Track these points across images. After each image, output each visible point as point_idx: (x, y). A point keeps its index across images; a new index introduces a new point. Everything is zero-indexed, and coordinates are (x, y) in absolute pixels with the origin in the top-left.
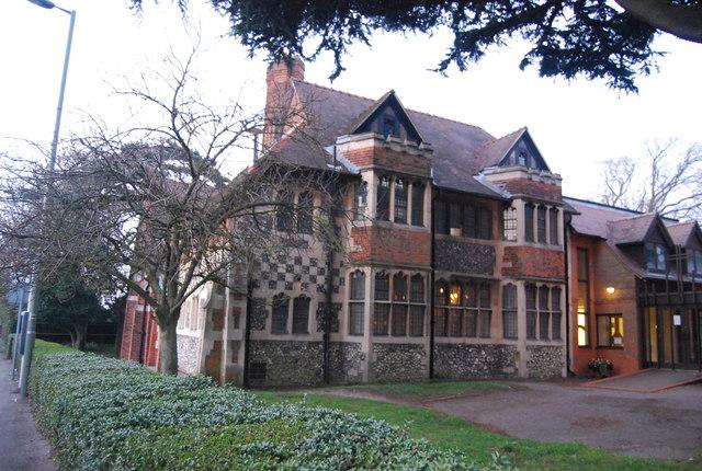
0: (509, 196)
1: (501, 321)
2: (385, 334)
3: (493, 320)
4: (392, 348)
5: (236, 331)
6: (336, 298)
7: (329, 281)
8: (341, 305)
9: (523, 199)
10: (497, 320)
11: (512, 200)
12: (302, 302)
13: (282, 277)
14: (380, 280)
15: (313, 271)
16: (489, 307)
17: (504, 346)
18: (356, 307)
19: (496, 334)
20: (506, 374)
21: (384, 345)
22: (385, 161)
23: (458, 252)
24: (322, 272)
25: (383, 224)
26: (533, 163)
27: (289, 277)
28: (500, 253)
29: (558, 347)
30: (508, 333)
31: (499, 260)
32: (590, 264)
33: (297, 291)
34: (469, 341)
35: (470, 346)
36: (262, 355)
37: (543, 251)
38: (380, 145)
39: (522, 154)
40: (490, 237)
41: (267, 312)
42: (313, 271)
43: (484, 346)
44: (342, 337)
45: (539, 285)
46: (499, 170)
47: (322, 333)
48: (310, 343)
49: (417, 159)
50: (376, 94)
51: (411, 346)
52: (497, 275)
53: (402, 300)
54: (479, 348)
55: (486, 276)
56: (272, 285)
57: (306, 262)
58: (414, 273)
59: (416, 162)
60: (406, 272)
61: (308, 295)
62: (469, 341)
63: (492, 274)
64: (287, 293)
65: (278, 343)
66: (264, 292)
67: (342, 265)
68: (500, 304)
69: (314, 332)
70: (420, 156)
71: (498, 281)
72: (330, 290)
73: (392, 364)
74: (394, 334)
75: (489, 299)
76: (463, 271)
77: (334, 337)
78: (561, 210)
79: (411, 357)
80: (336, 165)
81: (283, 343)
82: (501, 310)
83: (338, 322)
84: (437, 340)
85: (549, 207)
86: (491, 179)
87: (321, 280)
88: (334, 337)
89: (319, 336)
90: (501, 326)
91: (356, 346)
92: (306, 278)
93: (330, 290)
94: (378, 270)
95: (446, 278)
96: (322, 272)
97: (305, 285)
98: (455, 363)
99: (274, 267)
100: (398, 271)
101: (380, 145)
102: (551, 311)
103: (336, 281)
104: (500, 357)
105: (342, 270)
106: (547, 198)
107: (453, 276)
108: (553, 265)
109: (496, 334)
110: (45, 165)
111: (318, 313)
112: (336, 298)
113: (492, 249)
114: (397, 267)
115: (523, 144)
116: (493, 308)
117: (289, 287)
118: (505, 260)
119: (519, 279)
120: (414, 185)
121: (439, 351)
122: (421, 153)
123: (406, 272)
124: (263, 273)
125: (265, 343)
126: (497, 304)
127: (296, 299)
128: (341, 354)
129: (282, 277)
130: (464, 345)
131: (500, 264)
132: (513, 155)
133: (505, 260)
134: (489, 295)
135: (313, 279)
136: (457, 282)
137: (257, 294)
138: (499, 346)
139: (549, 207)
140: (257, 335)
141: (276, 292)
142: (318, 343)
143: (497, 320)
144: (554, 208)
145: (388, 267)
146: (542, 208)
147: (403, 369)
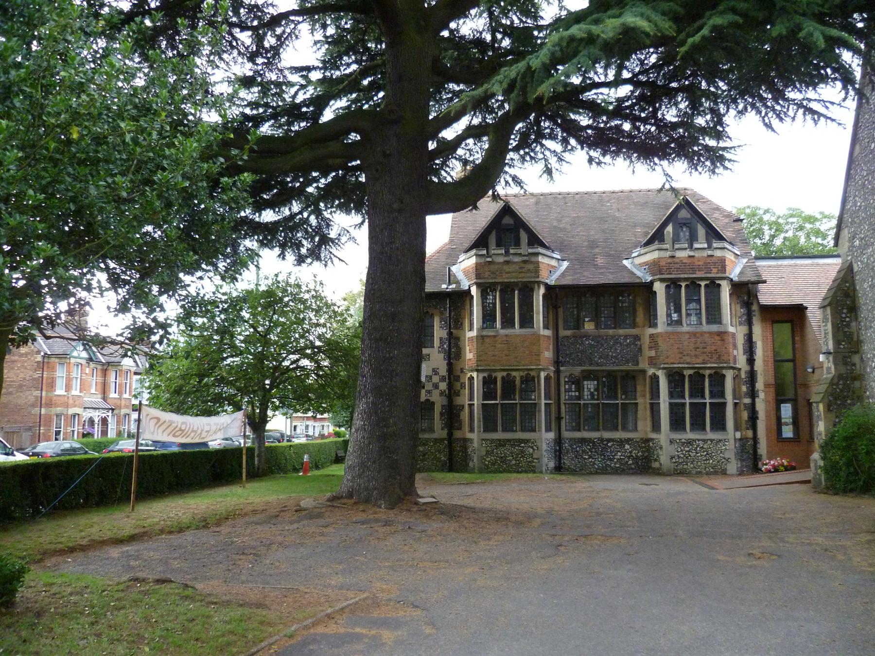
0: (649, 279)
1: (648, 412)
2: (495, 430)
4: (501, 443)
6: (458, 401)
7: (450, 386)
8: (463, 406)
9: (662, 280)
10: (644, 412)
11: (652, 283)
16: (636, 399)
17: (652, 440)
18: (654, 409)
21: (492, 441)
23: (591, 346)
24: (443, 379)
25: (489, 332)
26: (701, 231)
29: (720, 441)
32: (797, 338)
34: (607, 435)
35: (609, 440)
37: (694, 334)
38: (482, 260)
39: (681, 225)
40: (634, 325)
42: (436, 379)
46: (643, 251)
47: (446, 431)
48: (436, 439)
49: (523, 265)
52: (643, 364)
53: (531, 400)
54: (621, 442)
55: (630, 367)
60: (514, 374)
61: (432, 399)
62: (607, 435)
63: (637, 364)
68: (648, 396)
69: (439, 431)
70: (525, 262)
71: (644, 372)
72: (452, 393)
74: (505, 430)
75: (635, 391)
76: (598, 364)
79: (522, 452)
80: (450, 283)
87: (443, 386)
88: (458, 434)
89: (444, 434)
90: (649, 419)
91: (471, 440)
94: (486, 375)
96: (443, 379)
98: (590, 457)
100: (505, 374)
101: (482, 260)
102: (708, 401)
103: (457, 386)
104: (647, 447)
105: (462, 375)
107: (583, 371)
109: (644, 426)
110: (196, 58)
111: (441, 413)
112: (458, 401)
113: (637, 338)
115: (684, 214)
116: (640, 400)
119: (660, 369)
120: (520, 291)
121: (571, 446)
123: (514, 374)
126: (644, 396)
128: (465, 448)
130: (601, 440)
133: (650, 348)
134: (636, 388)
135: (436, 386)
138: (648, 440)
139: (703, 284)
142: (444, 439)
143: (644, 412)
147: (514, 462)
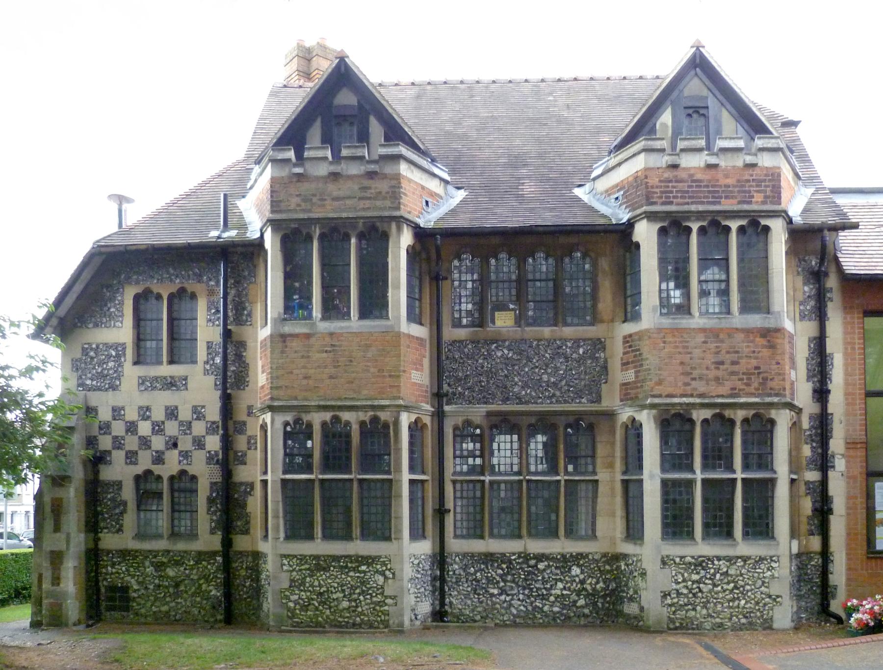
0: (624, 216)
1: (619, 500)
3: (602, 501)
4: (320, 564)
5: (58, 534)
7: (227, 443)
8: (252, 485)
9: (651, 217)
11: (630, 225)
12: (183, 483)
13: (145, 443)
14: (297, 433)
15: (199, 428)
16: (594, 473)
17: (625, 556)
19: (610, 528)
20: (628, 617)
21: (302, 559)
22: (295, 201)
23: (507, 361)
24: (212, 429)
27: (158, 443)
28: (617, 351)
30: (634, 530)
31: (615, 365)
33: (172, 464)
34: (536, 546)
35: (540, 557)
36: (115, 573)
37: (713, 334)
41: (125, 504)
43: (577, 558)
44: (254, 542)
45: (699, 415)
48: (200, 553)
49: (366, 183)
50: (667, 64)
51: (369, 560)
54: (565, 561)
55: (583, 405)
56: (131, 457)
57: (185, 414)
58: (366, 416)
59: (364, 189)
60: (346, 416)
61: (192, 470)
62: (536, 546)
63: (598, 400)
64: (157, 469)
65: (147, 554)
66: (118, 471)
67: (250, 414)
68: (619, 465)
70: (371, 175)
71: (610, 415)
72: (228, 460)
73: (321, 594)
74: (328, 536)
76: (520, 400)
77: (109, 541)
78: (777, 227)
81: (155, 553)
82: (619, 477)
83: (247, 515)
84: (455, 545)
85: (734, 225)
86: (600, 196)
87: (214, 443)
89: (215, 542)
90: (620, 512)
92: (186, 443)
93: (228, 460)
95: (477, 420)
97: (185, 455)
98: (503, 591)
99: (132, 428)
100: (327, 416)
101: (284, 172)
102: (739, 475)
105: (250, 421)
106: (727, 205)
107: (489, 414)
108: (745, 365)
109: (610, 528)
113: (599, 344)
114: (325, 408)
116: (602, 476)
117: (159, 459)
118: (625, 364)
119: (643, 407)
120: (361, 236)
121: (465, 568)
122: (372, 167)
123: (346, 416)
124: (115, 438)
125: (125, 554)
127: (172, 478)
129: (145, 443)
130: (525, 557)
131: (620, 375)
132: (666, 118)
133: (625, 364)
135: (199, 443)
136: (504, 423)
137: (108, 474)
139: (734, 225)
140: (109, 541)
141: (139, 469)
142: (214, 554)
144: (754, 223)
145: (306, 409)
146: (715, 228)
147: (345, 604)
